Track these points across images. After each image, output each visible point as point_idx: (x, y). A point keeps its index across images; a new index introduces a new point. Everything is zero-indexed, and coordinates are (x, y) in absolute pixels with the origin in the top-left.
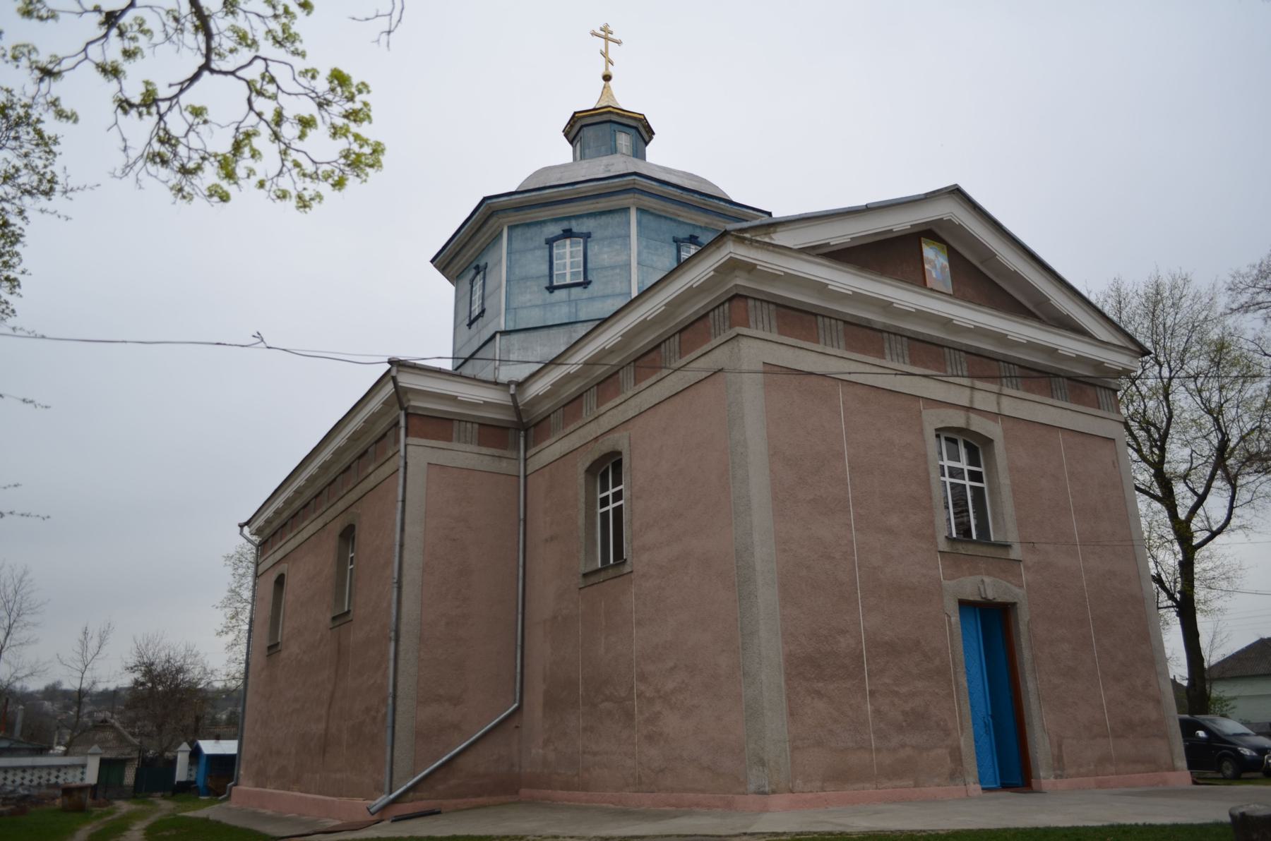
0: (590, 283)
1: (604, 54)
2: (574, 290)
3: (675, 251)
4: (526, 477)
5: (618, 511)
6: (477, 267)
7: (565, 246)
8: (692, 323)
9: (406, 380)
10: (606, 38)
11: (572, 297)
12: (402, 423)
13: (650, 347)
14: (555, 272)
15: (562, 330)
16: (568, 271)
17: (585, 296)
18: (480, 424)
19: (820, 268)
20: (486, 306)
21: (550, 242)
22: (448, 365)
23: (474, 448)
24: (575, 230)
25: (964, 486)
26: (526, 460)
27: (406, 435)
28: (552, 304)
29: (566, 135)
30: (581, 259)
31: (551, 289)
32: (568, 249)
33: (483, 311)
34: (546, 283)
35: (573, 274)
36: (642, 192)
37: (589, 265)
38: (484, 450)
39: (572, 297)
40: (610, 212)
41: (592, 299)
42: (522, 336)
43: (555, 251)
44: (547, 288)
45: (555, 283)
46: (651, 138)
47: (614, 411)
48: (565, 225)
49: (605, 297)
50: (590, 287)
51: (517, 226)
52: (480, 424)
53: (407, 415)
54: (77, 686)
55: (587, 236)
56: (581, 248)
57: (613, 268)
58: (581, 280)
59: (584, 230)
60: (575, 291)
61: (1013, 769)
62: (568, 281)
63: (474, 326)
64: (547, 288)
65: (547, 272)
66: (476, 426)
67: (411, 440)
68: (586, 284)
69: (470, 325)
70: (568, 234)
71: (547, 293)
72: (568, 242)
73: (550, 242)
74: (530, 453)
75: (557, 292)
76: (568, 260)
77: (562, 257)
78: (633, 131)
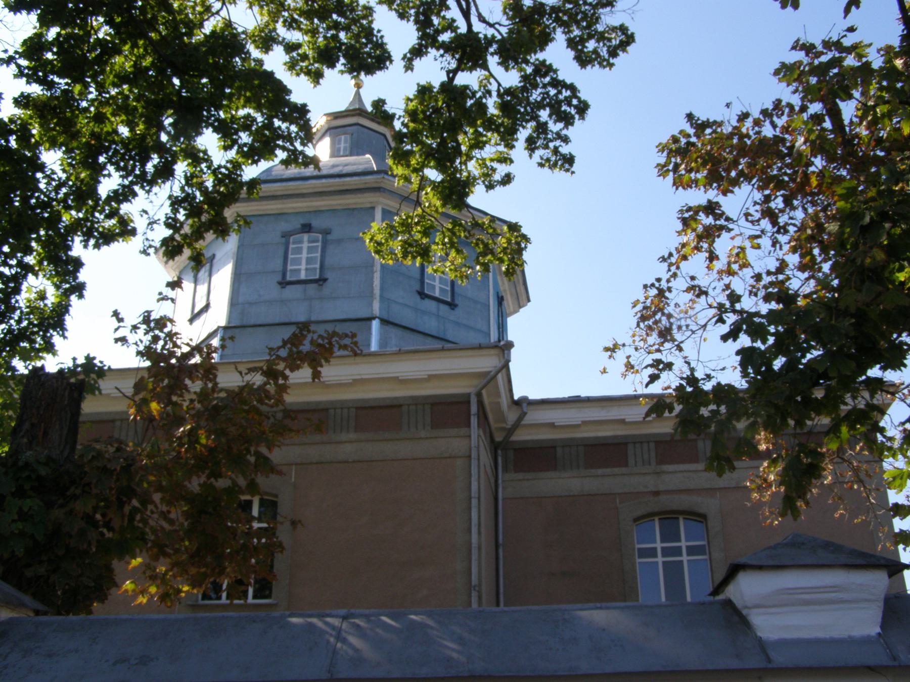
0: (325, 280)
7: (301, 242)
16: (303, 266)
19: (272, 210)
21: (286, 235)
22: (516, 397)
29: (514, 227)
31: (284, 283)
33: (207, 307)
34: (279, 278)
44: (280, 283)
45: (288, 278)
49: (468, 327)
54: (888, 412)
60: (312, 289)
61: (498, 605)
62: (303, 276)
64: (280, 283)
69: (191, 321)
70: (307, 228)
72: (306, 237)
77: (299, 251)
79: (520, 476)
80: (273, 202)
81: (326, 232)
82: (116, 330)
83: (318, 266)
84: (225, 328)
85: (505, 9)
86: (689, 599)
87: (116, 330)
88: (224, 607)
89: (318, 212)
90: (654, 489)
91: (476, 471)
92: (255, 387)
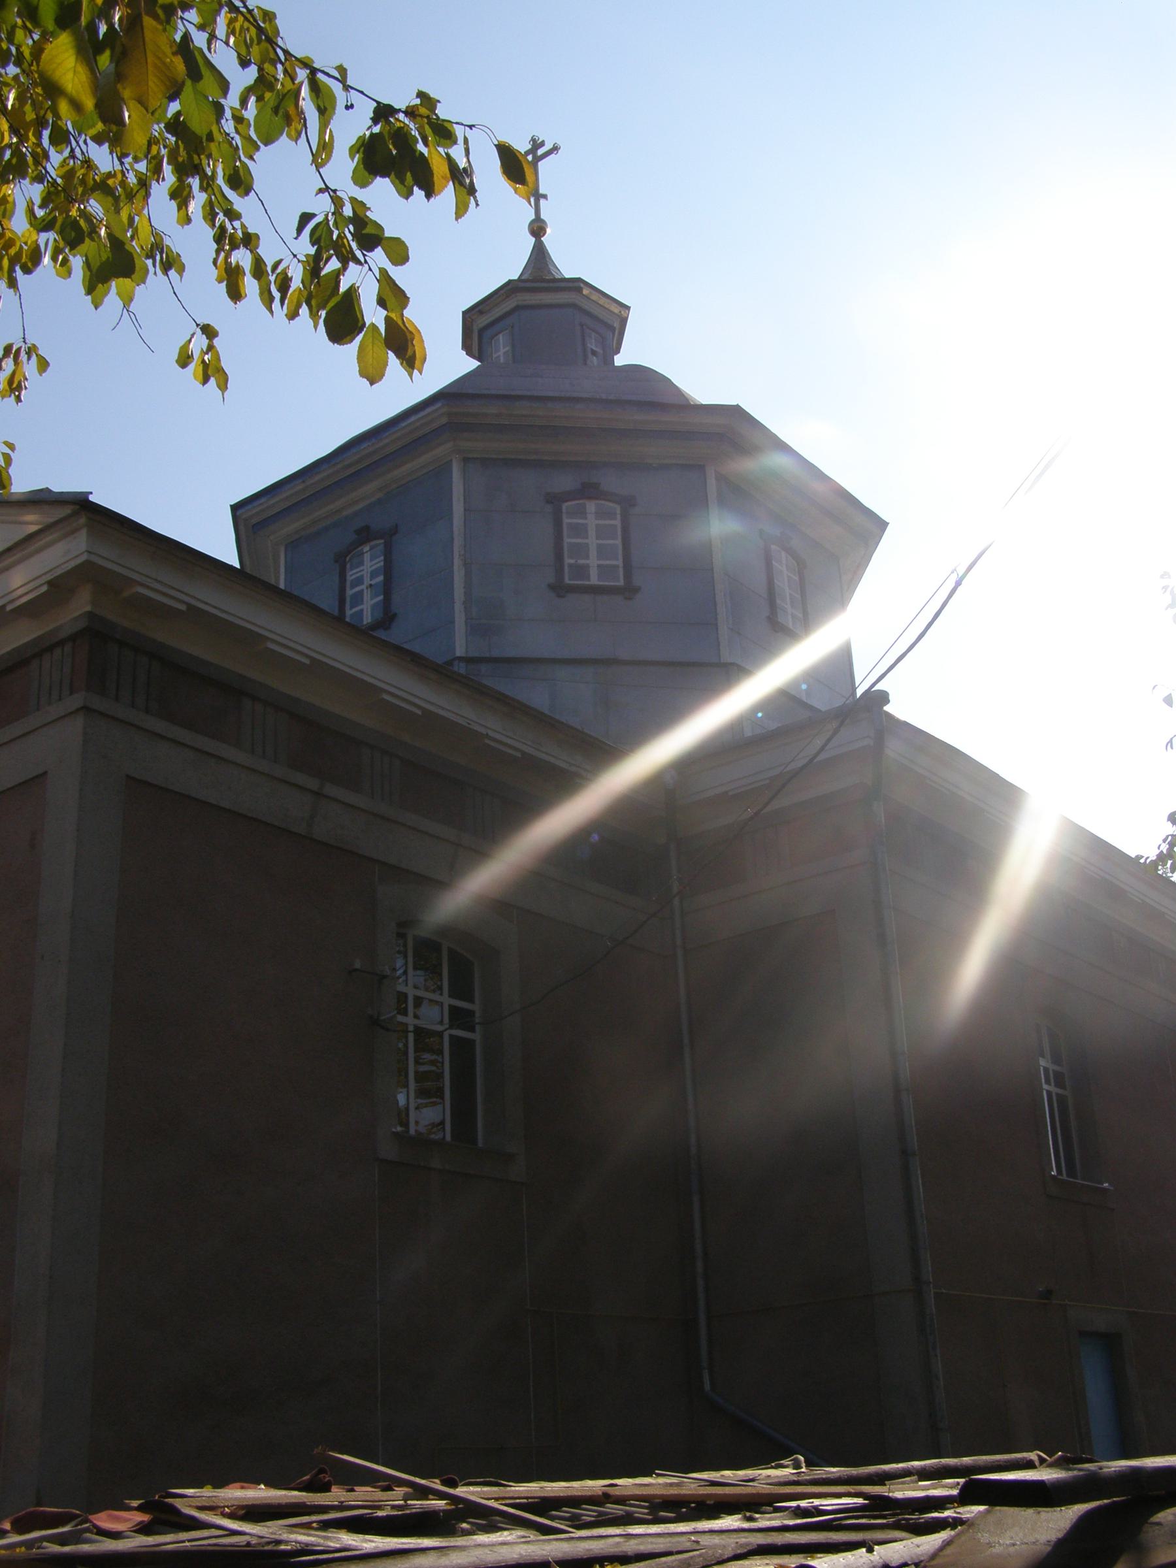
0: (636, 590)
31: (559, 589)
44: (552, 587)
55: (628, 503)
56: (617, 522)
62: (594, 580)
64: (552, 587)
72: (591, 506)
73: (555, 500)
81: (628, 503)
83: (620, 562)
86: (480, 1144)
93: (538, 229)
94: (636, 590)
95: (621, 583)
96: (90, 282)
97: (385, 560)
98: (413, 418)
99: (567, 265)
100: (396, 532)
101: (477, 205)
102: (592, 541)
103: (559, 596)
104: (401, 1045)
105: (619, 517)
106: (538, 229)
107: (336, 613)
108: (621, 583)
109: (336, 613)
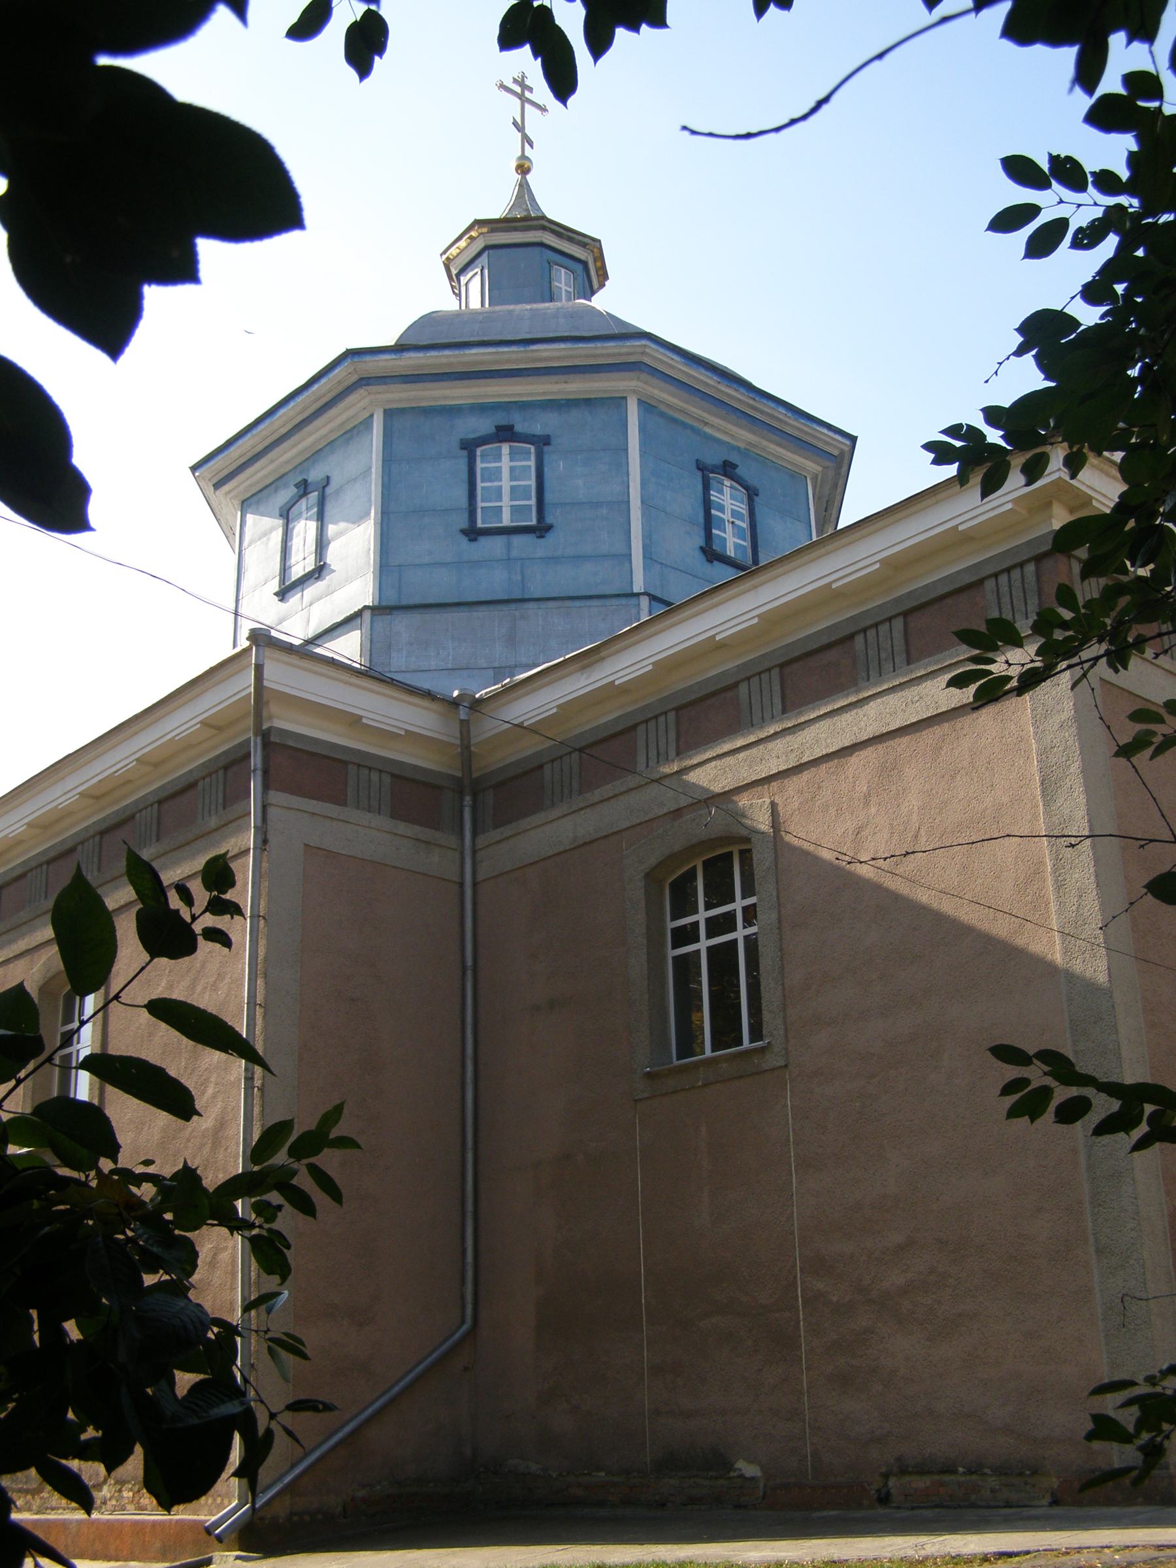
0: (549, 528)
1: (520, 127)
2: (518, 540)
3: (700, 487)
4: (475, 884)
5: (723, 958)
6: (304, 488)
7: (498, 458)
8: (941, 598)
9: (279, 676)
10: (521, 97)
11: (515, 553)
12: (256, 760)
13: (825, 640)
14: (480, 504)
15: (496, 612)
16: (506, 503)
17: (540, 553)
18: (393, 775)
20: (331, 557)
21: (469, 447)
23: (383, 821)
24: (519, 428)
25: (709, 949)
26: (474, 852)
27: (266, 787)
28: (476, 564)
30: (532, 482)
31: (473, 533)
32: (505, 463)
33: (319, 571)
34: (464, 523)
35: (515, 510)
36: (654, 371)
37: (549, 497)
38: (402, 828)
39: (515, 553)
40: (588, 403)
41: (554, 560)
42: (416, 618)
43: (480, 465)
44: (464, 532)
45: (480, 524)
46: (602, 286)
47: (729, 760)
48: (501, 419)
49: (579, 559)
50: (551, 537)
51: (402, 411)
52: (393, 775)
53: (267, 745)
55: (542, 442)
56: (532, 463)
57: (596, 505)
58: (534, 522)
59: (538, 429)
62: (506, 520)
63: (294, 599)
64: (464, 532)
65: (464, 502)
66: (387, 779)
67: (275, 797)
68: (541, 530)
70: (505, 433)
71: (464, 540)
72: (505, 448)
73: (469, 447)
74: (482, 840)
75: (484, 541)
76: (506, 484)
78: (579, 268)
79: (507, 831)
80: (436, 385)
82: (543, 109)
84: (377, 610)
85: (600, 258)
87: (543, 109)
88: (748, 1052)
89: (524, 406)
90: (674, 807)
91: (774, 766)
92: (1002, 433)
93: (523, 168)
94: (549, 528)
95: (534, 522)
96: (1149, 1500)
97: (730, 557)
98: (825, 431)
99: (554, 208)
100: (328, 484)
101: (502, 87)
102: (506, 484)
103: (470, 540)
104: (125, 1553)
105: (533, 457)
106: (523, 168)
107: (527, 106)
108: (534, 522)
109: (527, 106)
